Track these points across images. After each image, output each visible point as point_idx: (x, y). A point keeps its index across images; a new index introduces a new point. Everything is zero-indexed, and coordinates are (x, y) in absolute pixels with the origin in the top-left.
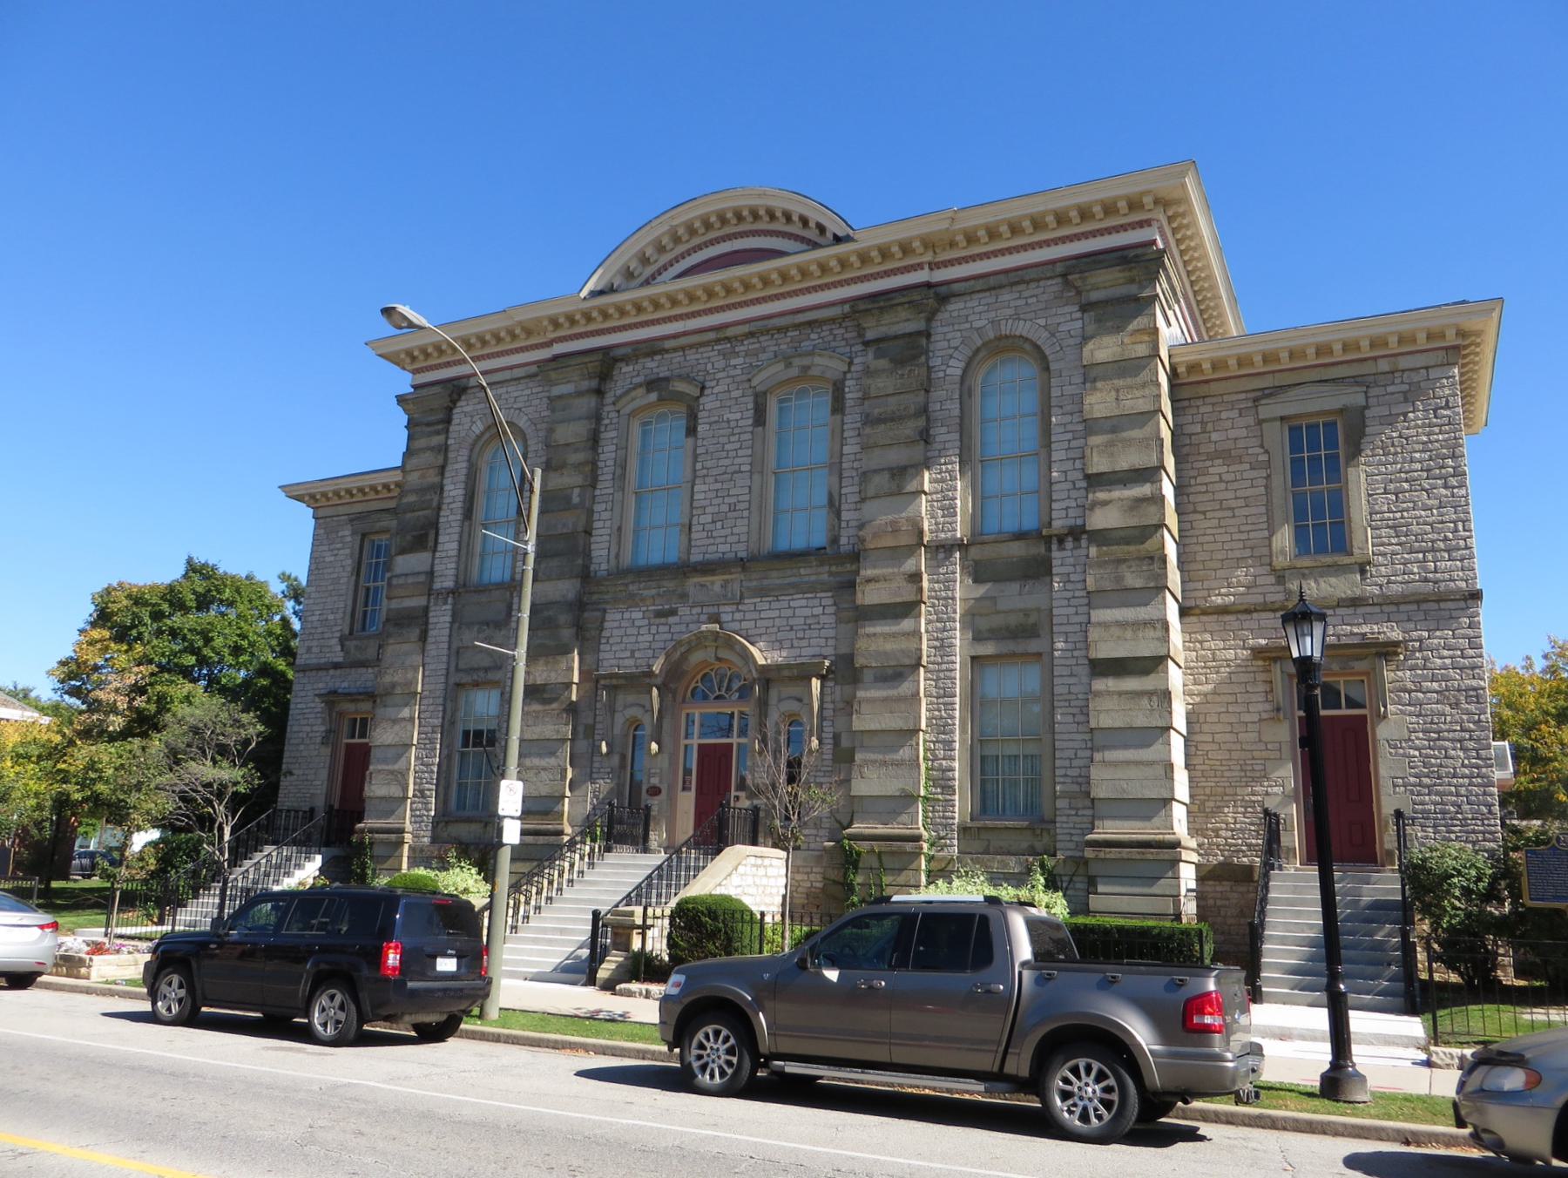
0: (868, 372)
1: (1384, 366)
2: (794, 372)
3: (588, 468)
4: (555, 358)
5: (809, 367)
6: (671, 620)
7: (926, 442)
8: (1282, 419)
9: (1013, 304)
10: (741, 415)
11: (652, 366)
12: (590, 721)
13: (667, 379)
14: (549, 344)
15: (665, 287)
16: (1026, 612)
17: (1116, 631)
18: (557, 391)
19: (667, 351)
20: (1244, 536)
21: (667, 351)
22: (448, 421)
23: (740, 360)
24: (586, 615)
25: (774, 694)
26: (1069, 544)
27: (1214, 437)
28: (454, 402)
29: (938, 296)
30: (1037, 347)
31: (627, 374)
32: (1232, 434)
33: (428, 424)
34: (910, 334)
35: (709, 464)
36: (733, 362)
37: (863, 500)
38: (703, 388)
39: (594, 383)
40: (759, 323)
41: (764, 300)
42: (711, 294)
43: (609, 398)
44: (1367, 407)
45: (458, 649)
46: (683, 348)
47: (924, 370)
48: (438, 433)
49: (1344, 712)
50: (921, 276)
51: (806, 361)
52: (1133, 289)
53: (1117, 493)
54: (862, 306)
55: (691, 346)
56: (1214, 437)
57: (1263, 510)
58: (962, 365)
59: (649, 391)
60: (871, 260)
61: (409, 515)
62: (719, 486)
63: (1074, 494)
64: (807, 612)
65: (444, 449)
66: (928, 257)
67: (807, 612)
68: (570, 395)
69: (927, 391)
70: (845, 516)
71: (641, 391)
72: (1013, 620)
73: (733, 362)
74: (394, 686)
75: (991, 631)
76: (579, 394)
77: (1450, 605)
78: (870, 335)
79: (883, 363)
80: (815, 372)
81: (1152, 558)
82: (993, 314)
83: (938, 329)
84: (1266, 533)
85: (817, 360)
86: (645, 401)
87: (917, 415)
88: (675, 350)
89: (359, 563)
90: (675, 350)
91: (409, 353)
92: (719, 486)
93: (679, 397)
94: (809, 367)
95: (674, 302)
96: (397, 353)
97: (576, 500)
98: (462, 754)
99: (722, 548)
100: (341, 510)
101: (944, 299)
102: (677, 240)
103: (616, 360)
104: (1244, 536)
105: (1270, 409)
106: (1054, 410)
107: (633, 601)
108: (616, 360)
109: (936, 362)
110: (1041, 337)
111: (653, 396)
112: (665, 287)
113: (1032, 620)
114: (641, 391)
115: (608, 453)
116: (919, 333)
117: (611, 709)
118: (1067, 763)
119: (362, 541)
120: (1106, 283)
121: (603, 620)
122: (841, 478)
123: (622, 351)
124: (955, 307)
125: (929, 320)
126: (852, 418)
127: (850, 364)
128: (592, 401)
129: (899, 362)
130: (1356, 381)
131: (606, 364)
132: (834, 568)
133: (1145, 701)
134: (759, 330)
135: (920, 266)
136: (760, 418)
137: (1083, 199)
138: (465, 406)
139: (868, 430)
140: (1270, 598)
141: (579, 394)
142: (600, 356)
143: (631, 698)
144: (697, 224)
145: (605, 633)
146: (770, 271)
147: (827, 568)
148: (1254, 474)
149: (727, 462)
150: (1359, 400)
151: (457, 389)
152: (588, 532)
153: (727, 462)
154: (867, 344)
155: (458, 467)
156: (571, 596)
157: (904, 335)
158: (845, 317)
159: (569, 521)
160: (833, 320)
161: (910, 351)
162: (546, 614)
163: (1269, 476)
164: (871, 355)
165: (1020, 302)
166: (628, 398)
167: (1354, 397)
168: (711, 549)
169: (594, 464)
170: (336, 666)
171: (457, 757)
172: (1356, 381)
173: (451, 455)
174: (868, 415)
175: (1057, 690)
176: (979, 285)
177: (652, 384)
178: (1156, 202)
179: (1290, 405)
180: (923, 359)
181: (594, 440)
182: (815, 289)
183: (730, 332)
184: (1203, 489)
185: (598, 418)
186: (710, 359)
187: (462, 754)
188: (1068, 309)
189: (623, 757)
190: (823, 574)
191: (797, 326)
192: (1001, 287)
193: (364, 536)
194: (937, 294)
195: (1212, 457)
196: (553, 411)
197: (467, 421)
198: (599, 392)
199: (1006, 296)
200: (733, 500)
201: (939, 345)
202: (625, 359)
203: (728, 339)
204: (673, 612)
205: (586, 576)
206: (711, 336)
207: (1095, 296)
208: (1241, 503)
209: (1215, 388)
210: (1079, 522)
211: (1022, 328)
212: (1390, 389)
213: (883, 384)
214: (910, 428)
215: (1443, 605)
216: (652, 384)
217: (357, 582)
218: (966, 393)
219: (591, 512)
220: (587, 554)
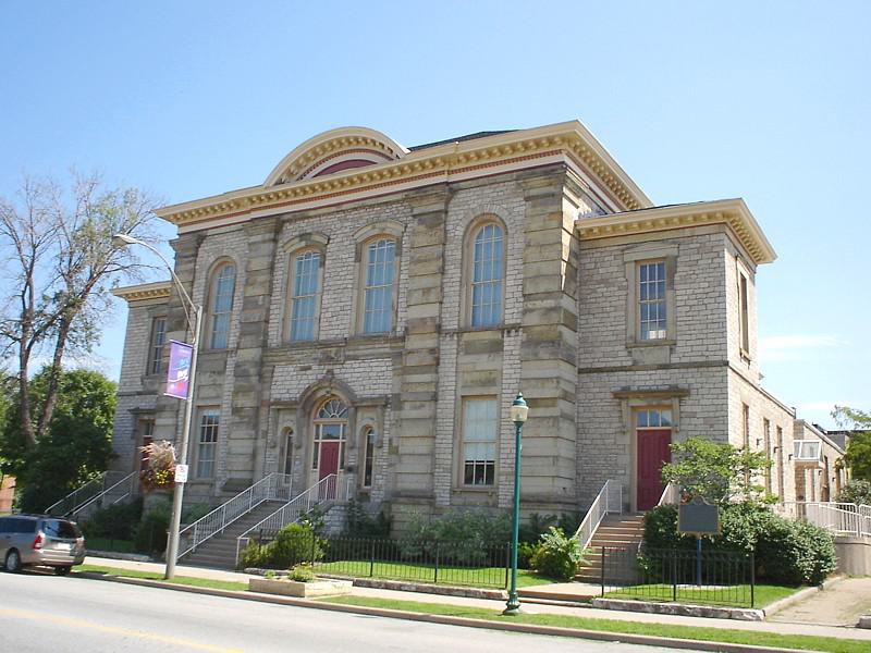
0: (414, 233)
1: (688, 232)
2: (376, 232)
3: (268, 284)
4: (252, 220)
5: (384, 229)
6: (309, 372)
7: (443, 274)
8: (636, 261)
9: (491, 195)
10: (348, 256)
11: (304, 226)
12: (265, 429)
13: (310, 234)
14: (248, 212)
15: (307, 182)
16: (491, 372)
17: (533, 382)
18: (253, 239)
19: (311, 217)
20: (613, 328)
21: (311, 217)
22: (196, 255)
23: (349, 224)
24: (264, 369)
25: (359, 414)
26: (513, 333)
27: (601, 271)
28: (199, 244)
29: (451, 189)
30: (502, 221)
31: (291, 230)
32: (610, 269)
33: (186, 257)
34: (436, 212)
35: (330, 284)
36: (346, 224)
37: (408, 306)
38: (329, 240)
39: (272, 236)
40: (361, 203)
41: (489, 165)
42: (402, 171)
43: (280, 245)
44: (677, 257)
45: (199, 386)
46: (320, 216)
47: (442, 233)
48: (190, 262)
49: (661, 428)
50: (443, 178)
51: (383, 225)
52: (552, 189)
53: (539, 304)
54: (412, 194)
55: (324, 215)
56: (601, 271)
57: (623, 313)
58: (463, 229)
59: (301, 241)
60: (542, 145)
61: (174, 309)
62: (335, 296)
63: (517, 305)
64: (379, 369)
65: (194, 271)
66: (446, 168)
67: (379, 369)
68: (259, 242)
69: (444, 244)
70: (400, 315)
71: (297, 240)
72: (483, 376)
73: (346, 224)
74: (165, 406)
75: (472, 382)
76: (264, 242)
77: (714, 369)
78: (416, 212)
79: (422, 228)
80: (387, 231)
81: (553, 342)
82: (480, 201)
83: (452, 208)
84: (624, 327)
85: (389, 225)
86: (299, 246)
87: (438, 258)
88: (315, 216)
89: (152, 334)
90: (315, 216)
91: (175, 216)
92: (335, 296)
93: (315, 245)
94: (384, 229)
95: (314, 190)
96: (169, 216)
97: (260, 303)
98: (202, 446)
99: (336, 332)
100: (146, 303)
101: (453, 192)
102: (308, 160)
103: (284, 222)
104: (613, 328)
105: (631, 256)
106: (509, 258)
107: (290, 361)
108: (284, 222)
109: (449, 227)
110: (504, 215)
111: (303, 244)
112: (307, 182)
113: (493, 376)
114: (297, 240)
115: (279, 275)
116: (440, 211)
117: (276, 423)
118: (505, 456)
119: (154, 321)
120: (539, 186)
121: (273, 372)
122: (398, 293)
123: (286, 217)
124: (461, 196)
125: (447, 203)
126: (405, 259)
127: (406, 227)
128: (271, 246)
129: (431, 227)
130: (674, 241)
131: (278, 224)
132: (393, 345)
133: (545, 422)
134: (361, 205)
135: (442, 173)
136: (358, 258)
137: (182, 210)
138: (205, 247)
139: (413, 267)
140: (624, 364)
141: (264, 242)
142: (274, 220)
143: (287, 417)
144: (327, 146)
145: (275, 379)
146: (334, 181)
147: (388, 345)
148: (621, 293)
149: (339, 282)
150: (674, 252)
151: (200, 237)
152: (267, 322)
153: (339, 282)
154: (414, 216)
155: (201, 282)
156: (257, 358)
157: (433, 212)
158: (404, 200)
159: (256, 315)
160: (398, 202)
161: (437, 220)
162: (243, 368)
163: (627, 295)
164: (416, 223)
165: (495, 194)
166: (289, 245)
167: (671, 251)
168: (331, 332)
169: (271, 282)
170: (139, 394)
171: (198, 448)
172: (674, 241)
173: (197, 275)
174: (412, 258)
175: (503, 415)
176: (474, 183)
177: (303, 236)
178: (563, 140)
179: (642, 253)
180: (442, 226)
181: (272, 268)
182: (532, 157)
183: (344, 207)
184: (593, 300)
185: (274, 255)
186: (331, 223)
187: (202, 446)
188: (518, 199)
189: (282, 449)
190: (386, 348)
191: (379, 205)
192: (485, 185)
193: (155, 318)
194: (451, 189)
195: (599, 283)
196: (250, 250)
197: (207, 255)
198: (275, 241)
199: (487, 190)
200: (342, 304)
201: (452, 217)
202: (289, 221)
203: (343, 211)
204: (310, 368)
205: (264, 346)
206: (334, 209)
207: (533, 192)
208: (612, 309)
209: (603, 243)
210: (519, 321)
211: (495, 209)
212: (692, 246)
213: (422, 240)
214: (434, 266)
215: (710, 369)
216: (303, 236)
217: (151, 345)
218: (465, 246)
219: (268, 310)
220: (266, 334)
